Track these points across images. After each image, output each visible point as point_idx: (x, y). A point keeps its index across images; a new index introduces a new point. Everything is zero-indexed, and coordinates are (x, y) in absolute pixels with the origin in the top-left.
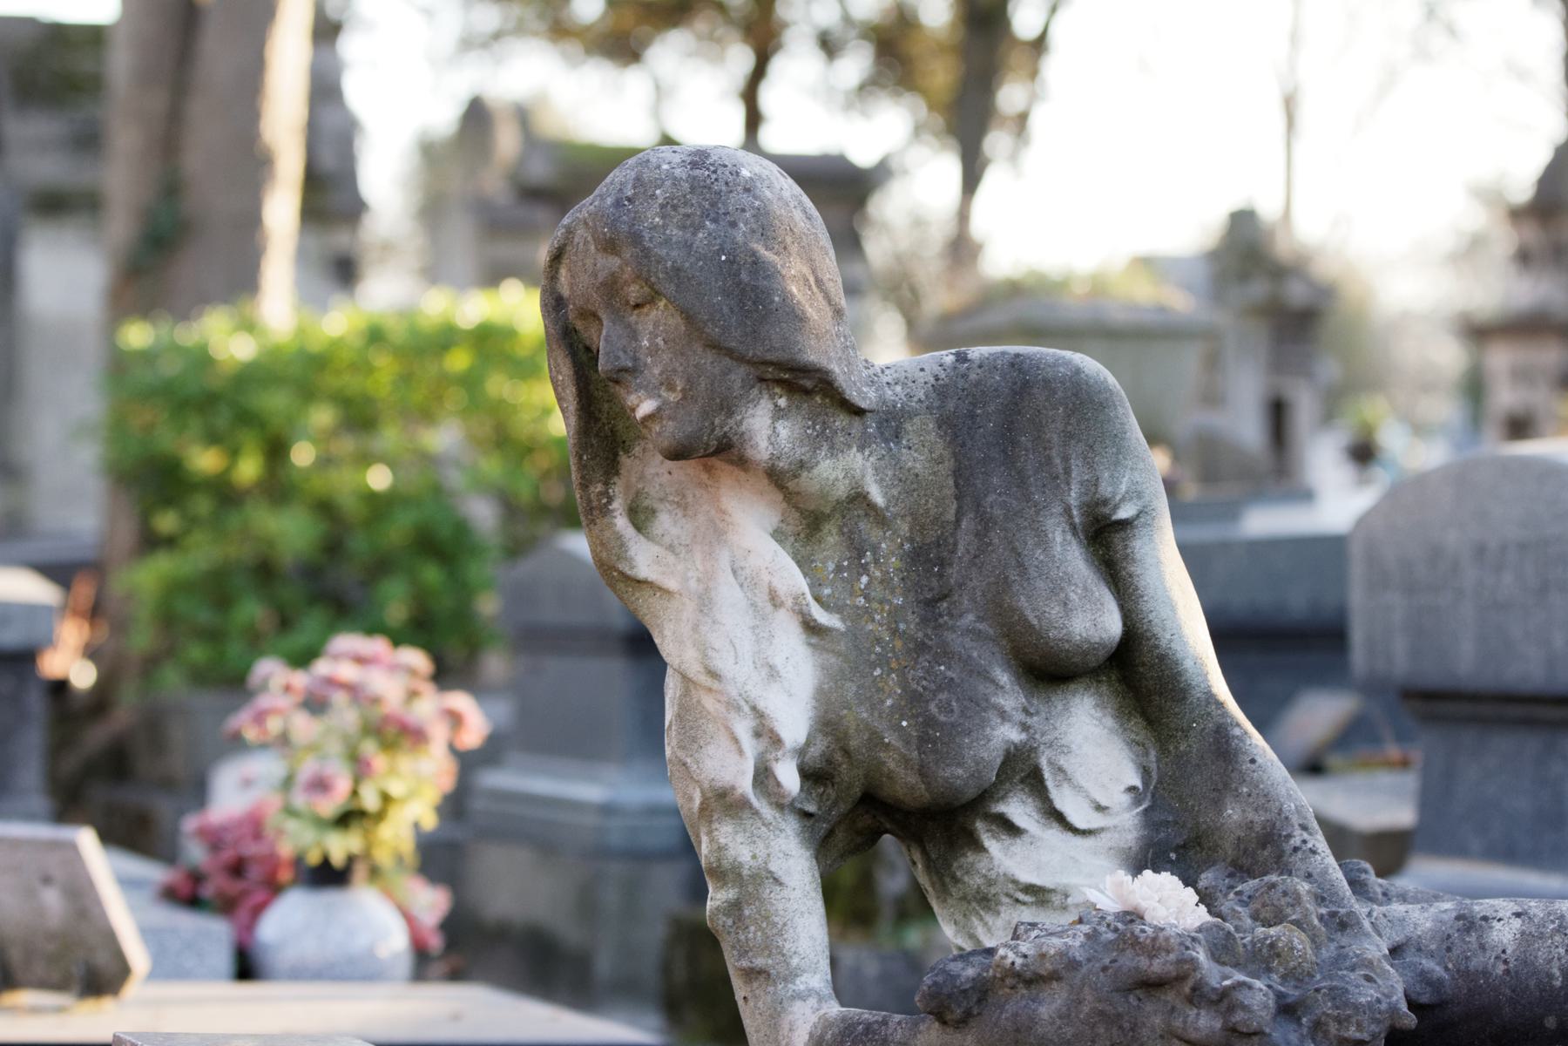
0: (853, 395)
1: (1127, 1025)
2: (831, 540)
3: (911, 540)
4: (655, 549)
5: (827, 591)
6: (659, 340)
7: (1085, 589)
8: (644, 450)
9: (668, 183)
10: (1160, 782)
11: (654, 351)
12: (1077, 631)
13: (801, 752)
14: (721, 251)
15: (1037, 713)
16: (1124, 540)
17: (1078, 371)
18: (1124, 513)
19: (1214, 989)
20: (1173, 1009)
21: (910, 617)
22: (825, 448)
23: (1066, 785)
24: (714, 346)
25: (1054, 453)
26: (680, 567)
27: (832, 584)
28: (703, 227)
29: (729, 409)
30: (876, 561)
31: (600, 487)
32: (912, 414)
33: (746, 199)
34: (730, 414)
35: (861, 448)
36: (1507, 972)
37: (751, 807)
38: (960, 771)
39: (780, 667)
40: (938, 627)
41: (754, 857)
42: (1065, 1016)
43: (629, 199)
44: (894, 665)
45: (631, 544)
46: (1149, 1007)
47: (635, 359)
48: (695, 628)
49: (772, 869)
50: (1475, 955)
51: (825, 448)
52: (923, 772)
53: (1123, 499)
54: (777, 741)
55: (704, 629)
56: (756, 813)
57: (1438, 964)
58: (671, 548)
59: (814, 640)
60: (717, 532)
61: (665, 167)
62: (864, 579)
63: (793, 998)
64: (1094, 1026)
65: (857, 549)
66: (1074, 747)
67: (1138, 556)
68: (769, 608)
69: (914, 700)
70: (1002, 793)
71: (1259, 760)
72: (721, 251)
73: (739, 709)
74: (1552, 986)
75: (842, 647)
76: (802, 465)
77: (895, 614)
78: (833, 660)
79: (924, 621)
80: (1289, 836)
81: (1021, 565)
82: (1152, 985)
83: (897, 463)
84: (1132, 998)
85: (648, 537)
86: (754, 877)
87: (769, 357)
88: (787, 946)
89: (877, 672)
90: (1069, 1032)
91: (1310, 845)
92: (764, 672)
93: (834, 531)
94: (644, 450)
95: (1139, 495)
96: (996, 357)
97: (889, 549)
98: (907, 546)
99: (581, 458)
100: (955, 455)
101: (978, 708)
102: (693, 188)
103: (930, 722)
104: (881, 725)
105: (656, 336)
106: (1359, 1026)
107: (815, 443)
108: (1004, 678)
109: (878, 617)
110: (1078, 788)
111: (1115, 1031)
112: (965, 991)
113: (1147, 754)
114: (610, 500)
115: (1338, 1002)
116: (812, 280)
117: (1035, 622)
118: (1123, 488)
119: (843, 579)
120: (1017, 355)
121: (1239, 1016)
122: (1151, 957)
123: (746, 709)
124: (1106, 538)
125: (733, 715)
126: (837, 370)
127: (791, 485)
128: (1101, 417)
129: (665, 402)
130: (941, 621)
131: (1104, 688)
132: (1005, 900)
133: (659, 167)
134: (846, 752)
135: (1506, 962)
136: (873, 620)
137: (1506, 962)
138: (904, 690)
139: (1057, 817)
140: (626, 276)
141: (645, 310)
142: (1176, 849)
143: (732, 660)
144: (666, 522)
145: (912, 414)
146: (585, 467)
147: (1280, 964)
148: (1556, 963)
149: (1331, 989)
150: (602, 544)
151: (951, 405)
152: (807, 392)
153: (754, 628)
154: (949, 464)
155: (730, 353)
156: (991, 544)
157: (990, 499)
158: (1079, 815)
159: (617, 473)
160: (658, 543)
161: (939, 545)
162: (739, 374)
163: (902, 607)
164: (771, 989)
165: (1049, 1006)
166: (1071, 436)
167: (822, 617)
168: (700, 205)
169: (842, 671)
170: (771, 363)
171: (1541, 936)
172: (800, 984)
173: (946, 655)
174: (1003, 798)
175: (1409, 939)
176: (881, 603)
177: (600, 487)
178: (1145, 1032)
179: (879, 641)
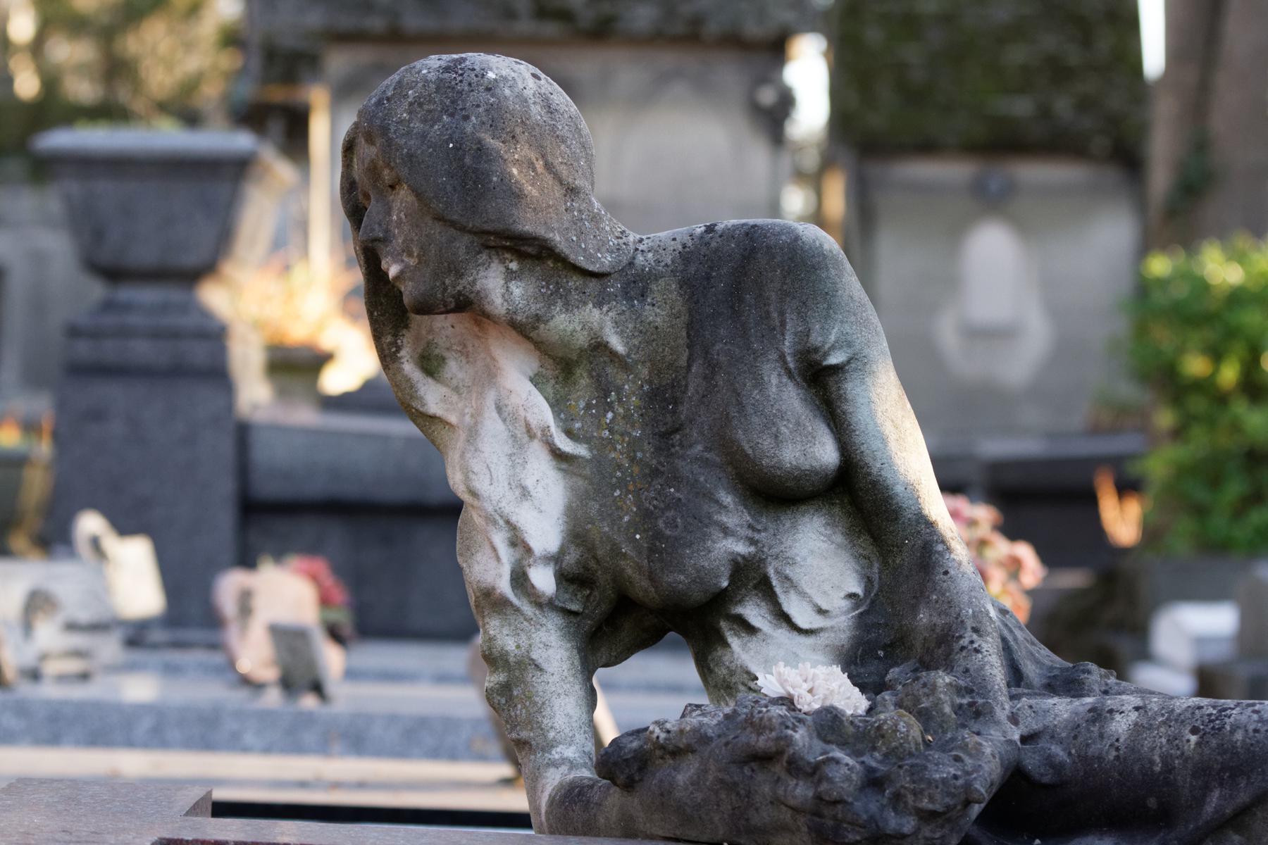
0: (581, 260)
1: (742, 792)
2: (583, 382)
3: (650, 382)
4: (443, 390)
5: (578, 425)
7: (798, 424)
10: (880, 590)
11: (400, 221)
12: (787, 459)
13: (555, 559)
14: (451, 139)
15: (765, 530)
18: (834, 359)
19: (809, 763)
20: (779, 779)
21: (646, 447)
22: (560, 303)
23: (792, 592)
24: (439, 218)
25: (772, 308)
27: (582, 419)
29: (457, 272)
30: (620, 400)
31: (389, 339)
32: (657, 277)
35: (599, 305)
36: (1117, 758)
37: (511, 604)
38: (682, 577)
39: (531, 488)
41: (518, 647)
42: (695, 783)
43: (388, 99)
44: (631, 488)
45: (420, 385)
46: (760, 777)
47: (387, 231)
48: (462, 456)
49: (534, 657)
50: (1094, 743)
51: (560, 303)
52: (652, 578)
53: (833, 348)
54: (529, 550)
56: (517, 610)
57: (1064, 750)
58: (456, 390)
59: (564, 466)
60: (490, 375)
62: (610, 415)
63: (548, 765)
64: (716, 793)
65: (603, 389)
66: (798, 559)
67: (849, 397)
68: (526, 439)
69: (646, 516)
70: (739, 597)
71: (952, 572)
72: (451, 139)
73: (495, 522)
74: (1153, 771)
75: (587, 472)
76: (538, 318)
77: (634, 444)
78: (580, 483)
79: (658, 450)
80: (961, 637)
81: (740, 403)
82: (763, 759)
84: (747, 770)
86: (519, 663)
88: (545, 721)
89: (617, 493)
90: (699, 796)
91: (975, 645)
93: (585, 375)
95: (849, 344)
97: (631, 389)
98: (646, 387)
100: (690, 311)
101: (701, 524)
102: (438, 88)
103: (658, 535)
104: (618, 538)
106: (931, 799)
107: (549, 301)
108: (727, 499)
109: (619, 447)
110: (803, 594)
111: (733, 797)
112: (626, 760)
113: (871, 566)
114: (399, 349)
115: (915, 777)
116: (539, 165)
117: (750, 452)
118: (832, 338)
120: (754, 226)
121: (824, 786)
122: (759, 734)
123: (501, 522)
124: (823, 383)
125: (491, 528)
126: (558, 238)
128: (813, 278)
129: (407, 266)
130: (673, 450)
131: (837, 510)
132: (742, 688)
134: (595, 557)
135: (1117, 749)
136: (615, 449)
137: (1117, 749)
138: (639, 508)
139: (784, 618)
142: (884, 648)
143: (487, 482)
144: (454, 368)
145: (657, 277)
147: (884, 743)
148: (1157, 752)
149: (912, 766)
151: (692, 269)
153: (511, 455)
154: (685, 318)
155: (453, 224)
156: (716, 386)
157: (717, 347)
158: (802, 615)
159: (407, 327)
160: (447, 386)
161: (673, 387)
162: (462, 244)
163: (640, 438)
164: (532, 757)
165: (684, 775)
166: (787, 294)
167: (566, 445)
169: (586, 491)
170: (488, 233)
171: (1150, 727)
172: (555, 754)
173: (676, 479)
174: (740, 602)
175: (1046, 728)
176: (622, 435)
177: (389, 339)
178: (758, 798)
179: (619, 467)
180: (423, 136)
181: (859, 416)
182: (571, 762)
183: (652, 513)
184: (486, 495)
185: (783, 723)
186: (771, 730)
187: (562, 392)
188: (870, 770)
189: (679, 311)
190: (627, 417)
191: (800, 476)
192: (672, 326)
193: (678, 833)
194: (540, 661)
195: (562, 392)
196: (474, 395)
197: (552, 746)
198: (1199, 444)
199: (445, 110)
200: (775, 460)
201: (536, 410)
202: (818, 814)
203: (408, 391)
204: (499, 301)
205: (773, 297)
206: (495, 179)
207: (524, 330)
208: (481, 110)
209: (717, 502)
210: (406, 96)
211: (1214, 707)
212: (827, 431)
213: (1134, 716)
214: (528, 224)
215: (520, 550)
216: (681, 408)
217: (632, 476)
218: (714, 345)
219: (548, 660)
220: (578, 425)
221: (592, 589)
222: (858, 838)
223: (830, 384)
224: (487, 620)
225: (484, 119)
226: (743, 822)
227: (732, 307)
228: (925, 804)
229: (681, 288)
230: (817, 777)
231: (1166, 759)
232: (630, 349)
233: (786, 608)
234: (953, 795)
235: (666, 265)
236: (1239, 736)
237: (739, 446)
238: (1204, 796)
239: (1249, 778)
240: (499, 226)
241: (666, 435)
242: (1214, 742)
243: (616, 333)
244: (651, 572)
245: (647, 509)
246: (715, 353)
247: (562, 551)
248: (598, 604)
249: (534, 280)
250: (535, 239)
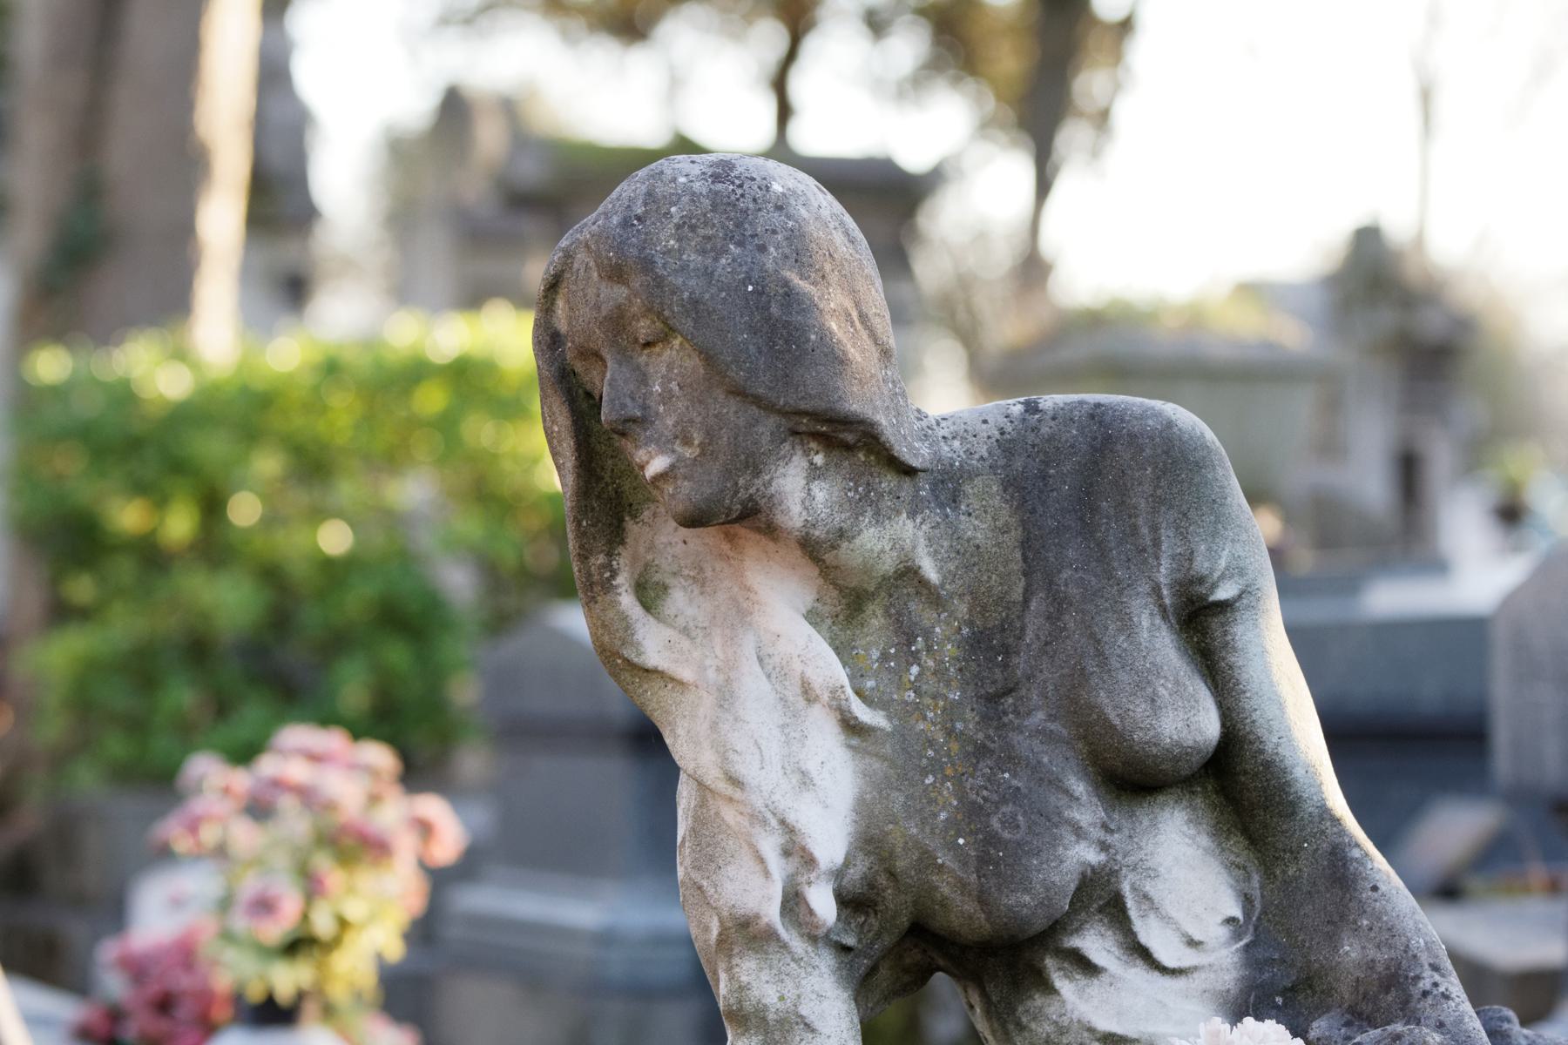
0: (903, 452)
2: (875, 622)
4: (667, 633)
5: (870, 684)
6: (674, 386)
7: (1177, 683)
9: (685, 199)
10: (1264, 912)
11: (667, 397)
13: (838, 874)
14: (748, 279)
15: (1119, 829)
17: (1170, 424)
18: (1223, 593)
21: (969, 715)
23: (1152, 916)
25: (1140, 521)
26: (696, 654)
29: (756, 467)
30: (929, 649)
31: (601, 559)
32: (972, 475)
33: (777, 219)
34: (757, 473)
35: (912, 515)
38: (1027, 898)
39: (814, 774)
40: (1002, 726)
41: (781, 998)
43: (639, 218)
44: (949, 772)
45: (638, 626)
47: (645, 407)
48: (714, 726)
49: (803, 1013)
51: (869, 513)
52: (982, 900)
53: (1222, 577)
54: (809, 861)
55: (724, 727)
56: (784, 946)
58: (685, 631)
59: (855, 742)
60: (741, 613)
61: (682, 180)
62: (915, 670)
65: (906, 634)
66: (1161, 869)
67: (1239, 645)
68: (801, 703)
69: (973, 812)
70: (1076, 924)
71: (1383, 888)
75: (887, 749)
76: (841, 534)
77: (951, 711)
78: (877, 765)
79: (985, 719)
80: (1418, 978)
81: (1100, 654)
83: (955, 533)
85: (659, 618)
86: (781, 1022)
87: (803, 406)
89: (930, 780)
91: (1442, 989)
92: (795, 779)
93: (879, 612)
95: (1242, 572)
96: (1072, 407)
97: (945, 634)
98: (965, 631)
99: (579, 524)
100: (1023, 523)
101: (1050, 824)
103: (992, 839)
104: (932, 843)
105: (670, 381)
108: (1079, 787)
109: (930, 715)
110: (1167, 919)
113: (1248, 879)
116: (855, 315)
117: (1117, 722)
118: (1223, 563)
119: (889, 669)
120: (1098, 405)
123: (774, 822)
124: (1201, 622)
125: (758, 830)
126: (884, 422)
129: (680, 459)
130: (1005, 719)
131: (1199, 801)
133: (674, 180)
134: (892, 875)
136: (925, 718)
138: (960, 801)
139: (1143, 954)
140: (634, 309)
141: (657, 349)
142: (1283, 993)
144: (679, 601)
145: (972, 475)
146: (584, 534)
150: (604, 626)
151: (1018, 464)
152: (848, 448)
153: (783, 726)
154: (1016, 534)
155: (757, 401)
156: (1065, 629)
157: (1064, 575)
158: (1167, 950)
160: (671, 626)
161: (1004, 630)
162: (767, 426)
163: (960, 703)
170: (805, 413)
173: (1010, 759)
174: (1077, 931)
176: (934, 697)
177: (601, 559)
179: (931, 743)
183: (981, 807)
189: (1007, 524)
190: (939, 672)
191: (1179, 754)
192: (998, 545)
194: (812, 1018)
196: (718, 641)
198: (122, 628)
200: (1152, 733)
203: (621, 634)
205: (1143, 504)
206: (813, 337)
207: (815, 551)
208: (779, 237)
209: (1067, 792)
210: (667, 214)
212: (1208, 693)
215: (795, 861)
216: (1015, 660)
217: (949, 756)
218: (1059, 572)
220: (870, 684)
221: (867, 914)
223: (1214, 626)
224: (736, 960)
225: (787, 251)
227: (1081, 519)
232: (945, 577)
233: (1144, 939)
235: (982, 458)
237: (1102, 714)
240: (819, 405)
241: (993, 699)
243: (929, 554)
244: (981, 892)
245: (974, 803)
246: (1061, 582)
247: (847, 864)
248: (879, 935)
249: (839, 479)
250: (862, 422)
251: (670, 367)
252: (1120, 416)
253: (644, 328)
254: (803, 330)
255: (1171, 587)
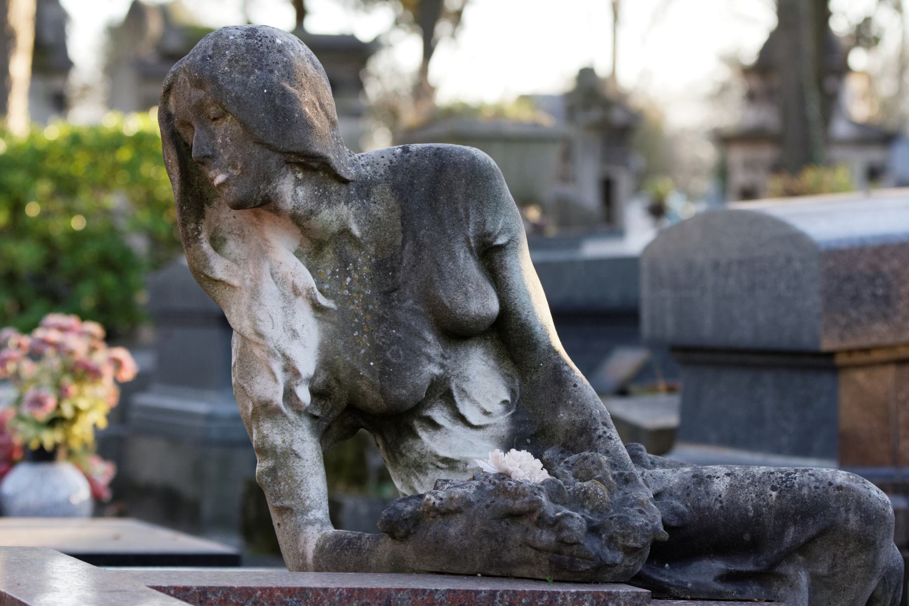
2: (329, 256)
3: (376, 256)
4: (226, 262)
5: (327, 286)
6: (228, 139)
7: (478, 285)
8: (219, 204)
10: (521, 398)
11: (224, 145)
13: (311, 380)
14: (264, 87)
15: (450, 358)
16: (500, 257)
18: (501, 241)
19: (551, 518)
20: (527, 530)
21: (375, 301)
24: (259, 142)
26: (240, 272)
27: (330, 282)
28: (254, 73)
29: (269, 180)
31: (193, 226)
32: (376, 183)
33: (278, 56)
34: (269, 183)
35: (347, 203)
36: (722, 507)
39: (299, 331)
40: (391, 307)
41: (284, 442)
42: (464, 534)
43: (210, 57)
44: (366, 330)
46: (513, 528)
47: (213, 150)
48: (249, 308)
51: (325, 202)
52: (382, 392)
53: (500, 233)
54: (297, 374)
55: (254, 308)
56: (285, 416)
57: (682, 503)
58: (235, 261)
59: (319, 315)
60: (262, 252)
61: (231, 37)
62: (348, 279)
65: (344, 262)
66: (471, 377)
67: (508, 266)
68: (293, 296)
69: (377, 350)
70: (429, 404)
71: (579, 385)
73: (275, 355)
74: (747, 516)
75: (335, 319)
76: (311, 212)
77: (366, 300)
78: (330, 326)
79: (383, 304)
80: (596, 429)
81: (440, 271)
82: (514, 516)
83: (368, 212)
84: (503, 523)
86: (283, 453)
87: (292, 149)
88: (303, 494)
89: (356, 334)
93: (331, 251)
94: (219, 204)
97: (363, 262)
98: (373, 260)
99: (182, 208)
100: (402, 207)
101: (415, 355)
102: (247, 52)
103: (387, 363)
104: (357, 365)
106: (635, 540)
107: (319, 199)
108: (430, 337)
109: (356, 302)
110: (473, 402)
111: (493, 542)
112: (406, 520)
113: (513, 382)
114: (199, 233)
116: (317, 104)
117: (448, 304)
119: (336, 279)
120: (438, 149)
121: (565, 534)
122: (515, 499)
123: (279, 355)
124: (490, 256)
125: (271, 359)
126: (332, 157)
127: (305, 224)
129: (231, 176)
130: (393, 304)
131: (489, 343)
132: (431, 466)
133: (228, 38)
135: (721, 502)
136: (353, 303)
137: (721, 502)
138: (371, 344)
139: (461, 419)
142: (531, 437)
143: (270, 326)
144: (232, 246)
145: (376, 183)
147: (590, 503)
148: (750, 503)
149: (619, 518)
150: (195, 259)
151: (399, 178)
152: (315, 170)
153: (284, 308)
154: (398, 212)
155: (269, 147)
156: (421, 259)
157: (422, 233)
158: (474, 417)
159: (203, 217)
160: (228, 258)
161: (392, 260)
162: (274, 159)
163: (370, 296)
164: (294, 519)
165: (455, 528)
166: (469, 196)
167: (323, 301)
168: (252, 60)
169: (335, 333)
170: (293, 153)
171: (742, 487)
172: (311, 516)
173: (396, 324)
174: (430, 407)
175: (665, 489)
176: (358, 293)
177: (193, 226)
179: (357, 315)
180: (244, 84)
181: (514, 280)
182: (321, 521)
183: (382, 347)
184: (269, 336)
185: (532, 492)
186: (524, 496)
187: (313, 263)
188: (589, 522)
190: (361, 281)
192: (389, 218)
193: (444, 568)
195: (313, 263)
197: (309, 511)
199: (255, 66)
201: (302, 276)
202: (559, 553)
204: (289, 200)
205: (460, 197)
207: (299, 221)
208: (280, 66)
209: (424, 339)
211: (782, 473)
213: (728, 480)
214: (318, 148)
215: (290, 374)
216: (398, 274)
217: (365, 321)
219: (304, 450)
222: (588, 567)
223: (496, 257)
225: (284, 73)
226: (497, 559)
228: (631, 543)
229: (393, 191)
230: (557, 527)
231: (756, 508)
233: (462, 411)
234: (647, 537)
235: (381, 175)
236: (805, 491)
238: (783, 531)
239: (815, 519)
242: (789, 496)
244: (382, 389)
247: (315, 375)
248: (331, 410)
251: (226, 130)
252: (449, 154)
253: (213, 111)
254: (292, 112)
255: (474, 238)
